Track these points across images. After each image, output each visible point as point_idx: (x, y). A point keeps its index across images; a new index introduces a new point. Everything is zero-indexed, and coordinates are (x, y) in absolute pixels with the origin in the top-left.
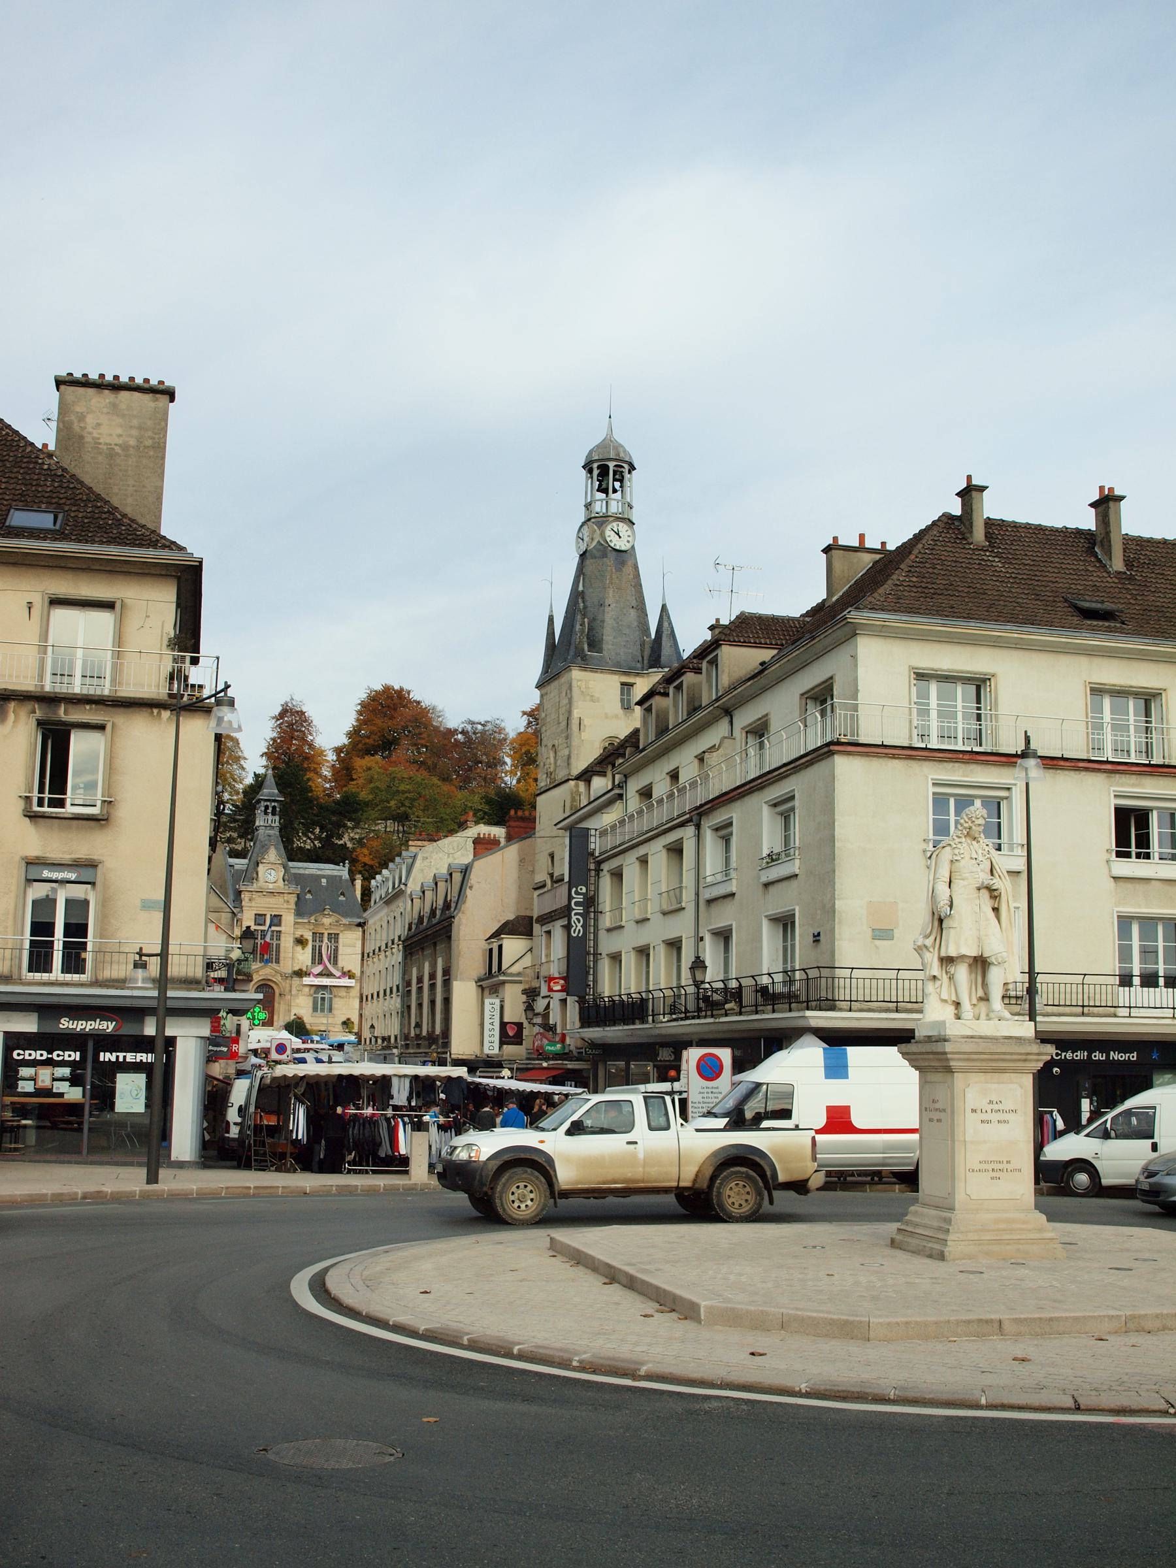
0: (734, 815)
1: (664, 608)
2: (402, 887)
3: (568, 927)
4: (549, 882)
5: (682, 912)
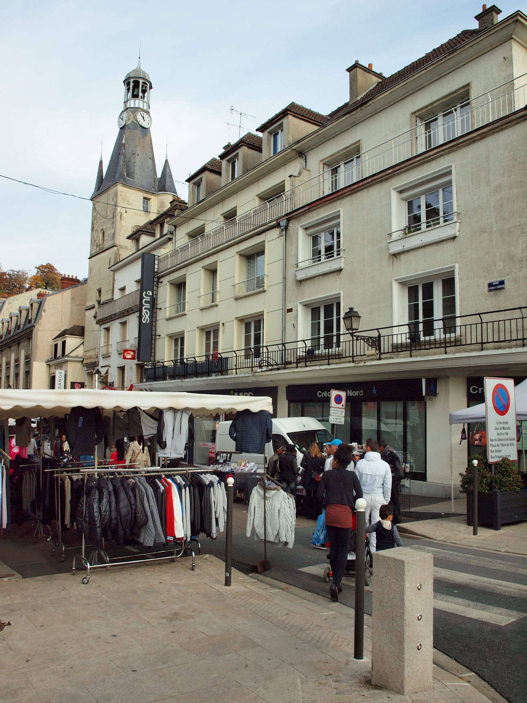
0: (341, 210)
1: (167, 162)
3: (140, 317)
4: (97, 305)
5: (184, 317)
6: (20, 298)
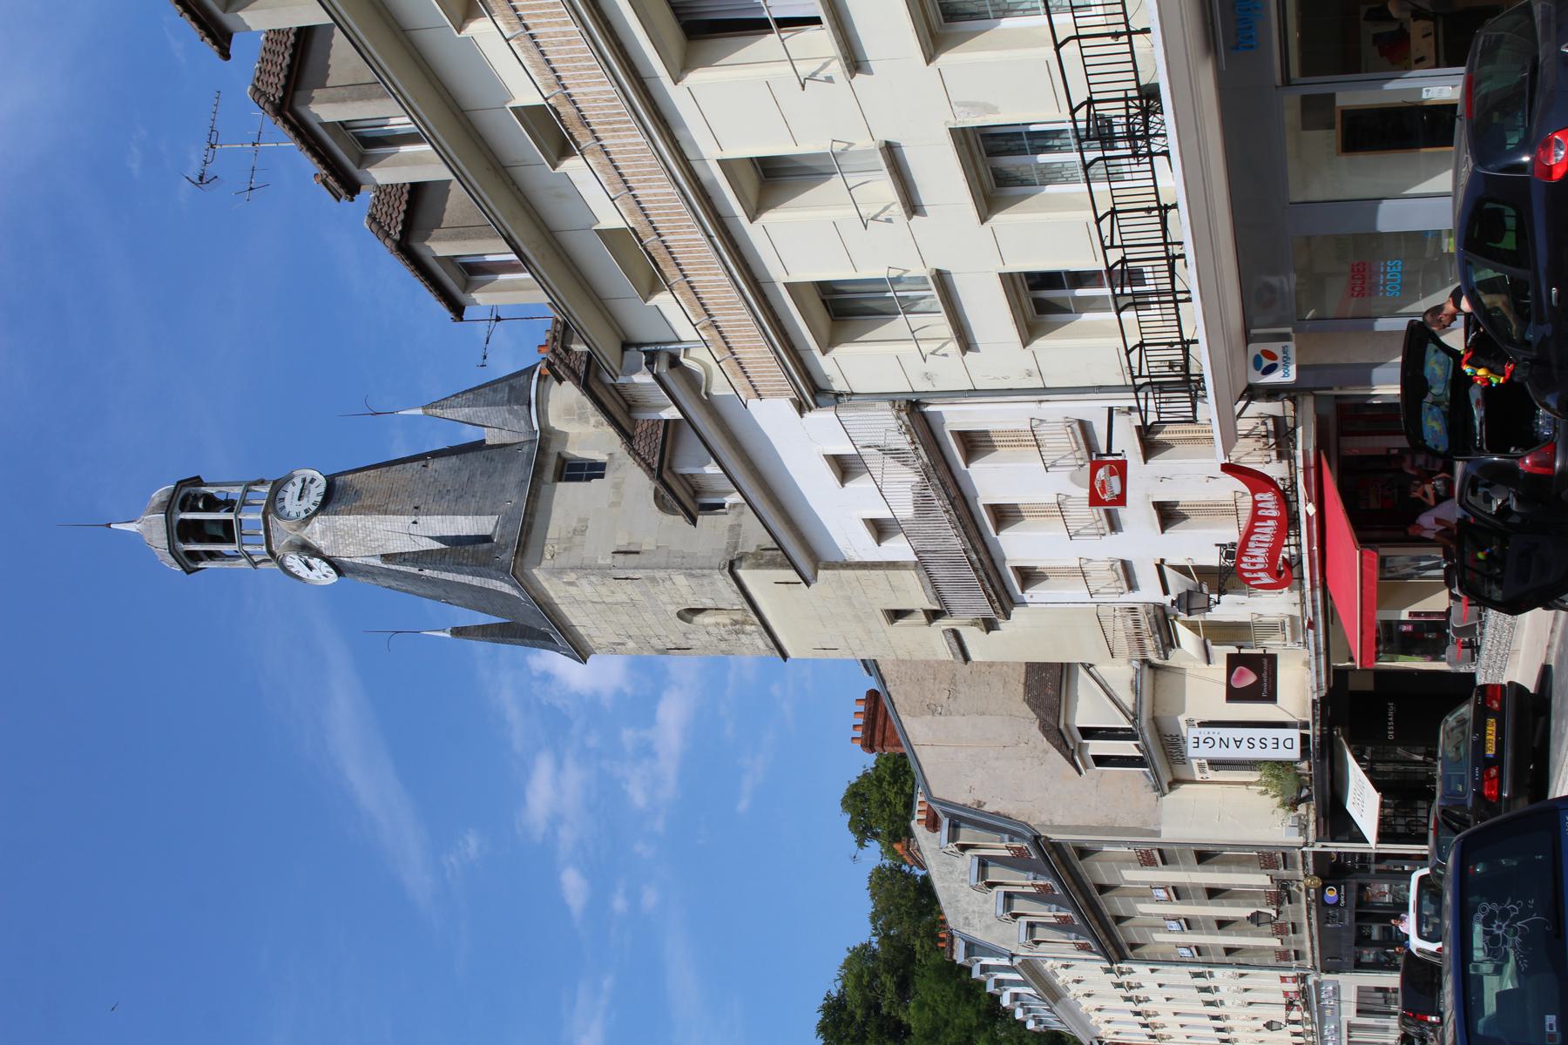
2: (1017, 961)
4: (944, 623)
6: (948, 889)
